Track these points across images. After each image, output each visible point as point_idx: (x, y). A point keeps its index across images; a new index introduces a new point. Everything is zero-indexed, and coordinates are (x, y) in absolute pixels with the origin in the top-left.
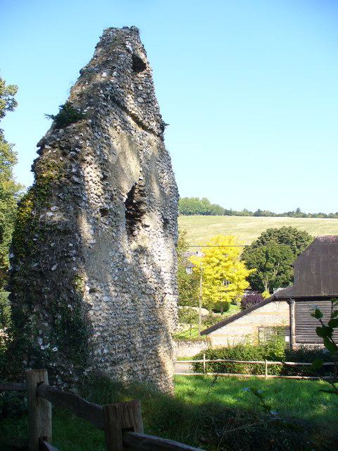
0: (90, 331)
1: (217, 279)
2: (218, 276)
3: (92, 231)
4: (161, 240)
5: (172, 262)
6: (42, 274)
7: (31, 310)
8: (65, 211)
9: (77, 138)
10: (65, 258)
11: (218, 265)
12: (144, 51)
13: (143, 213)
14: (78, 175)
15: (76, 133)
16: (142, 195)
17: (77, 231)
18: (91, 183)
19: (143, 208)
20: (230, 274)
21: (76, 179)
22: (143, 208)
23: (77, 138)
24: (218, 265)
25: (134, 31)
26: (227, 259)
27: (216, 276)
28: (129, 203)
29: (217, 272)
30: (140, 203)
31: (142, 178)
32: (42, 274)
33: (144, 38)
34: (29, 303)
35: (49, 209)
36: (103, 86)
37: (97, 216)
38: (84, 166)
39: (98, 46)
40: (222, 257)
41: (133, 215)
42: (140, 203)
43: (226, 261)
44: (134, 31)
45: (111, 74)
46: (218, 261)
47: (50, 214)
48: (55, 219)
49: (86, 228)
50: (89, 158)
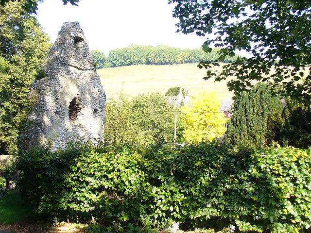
0: (176, 180)
1: (202, 124)
2: (202, 122)
3: (50, 121)
4: (92, 119)
5: (100, 128)
6: (29, 139)
7: (25, 151)
8: (38, 115)
9: (43, 85)
10: (37, 133)
11: (203, 113)
12: (82, 32)
13: (81, 109)
14: (43, 101)
15: (43, 83)
16: (80, 101)
17: (43, 122)
18: (49, 103)
19: (80, 106)
20: (212, 121)
21: (42, 103)
22: (80, 106)
23: (43, 85)
24: (203, 113)
25: (76, 25)
26: (209, 109)
27: (200, 123)
28: (73, 102)
29: (201, 119)
30: (79, 104)
31: (79, 94)
32: (29, 139)
33: (82, 26)
34: (24, 149)
35: (32, 115)
36: (57, 58)
37: (53, 115)
38: (46, 97)
39: (59, 33)
40: (205, 108)
41: (74, 108)
42: (79, 104)
43: (208, 112)
44: (76, 25)
45: (61, 52)
46: (202, 111)
47: (32, 116)
48: (34, 118)
49: (46, 120)
50: (48, 94)
